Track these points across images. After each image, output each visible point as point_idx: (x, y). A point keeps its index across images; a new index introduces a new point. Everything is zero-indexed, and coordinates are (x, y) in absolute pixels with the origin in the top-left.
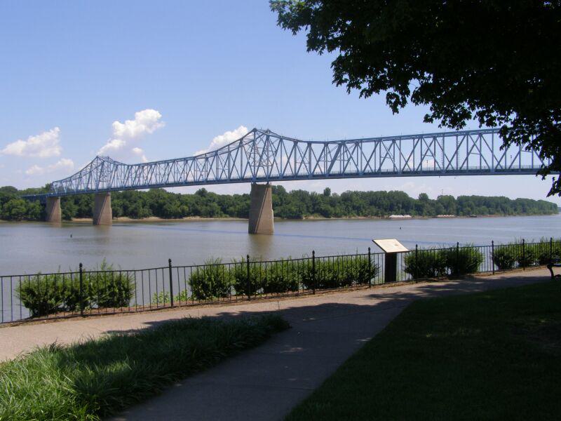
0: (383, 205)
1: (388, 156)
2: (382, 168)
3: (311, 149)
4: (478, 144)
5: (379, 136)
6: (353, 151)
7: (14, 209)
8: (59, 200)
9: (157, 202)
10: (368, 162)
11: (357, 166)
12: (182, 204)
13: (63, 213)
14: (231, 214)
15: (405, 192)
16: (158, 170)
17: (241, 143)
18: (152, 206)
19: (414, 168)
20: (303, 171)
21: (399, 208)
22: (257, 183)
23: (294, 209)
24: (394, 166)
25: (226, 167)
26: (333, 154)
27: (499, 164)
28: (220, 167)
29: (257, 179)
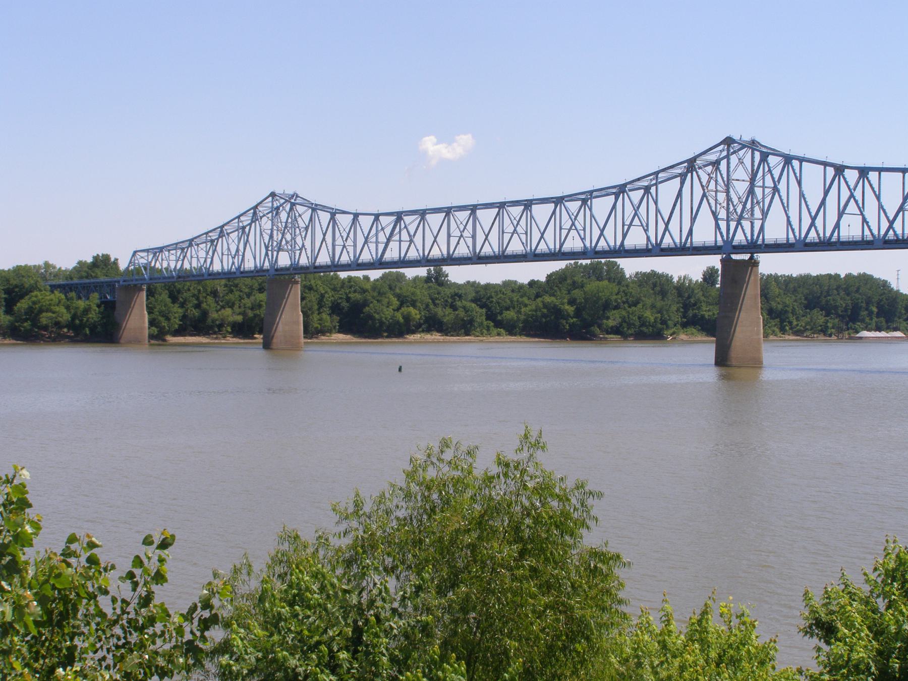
0: (836, 307)
1: (573, 228)
2: (626, 243)
3: (335, 223)
4: (858, 194)
5: (559, 194)
6: (417, 229)
7: (44, 314)
8: (144, 293)
9: (348, 299)
10: (602, 231)
11: (583, 239)
12: (402, 304)
13: (152, 323)
14: (511, 329)
15: (868, 273)
16: (194, 252)
17: (255, 213)
18: (335, 309)
19: (256, 267)
20: (516, 247)
21: (870, 313)
22: (734, 257)
23: (650, 316)
24: (648, 238)
25: (350, 242)
26: (388, 231)
27: (891, 226)
28: (339, 242)
29: (735, 247)
